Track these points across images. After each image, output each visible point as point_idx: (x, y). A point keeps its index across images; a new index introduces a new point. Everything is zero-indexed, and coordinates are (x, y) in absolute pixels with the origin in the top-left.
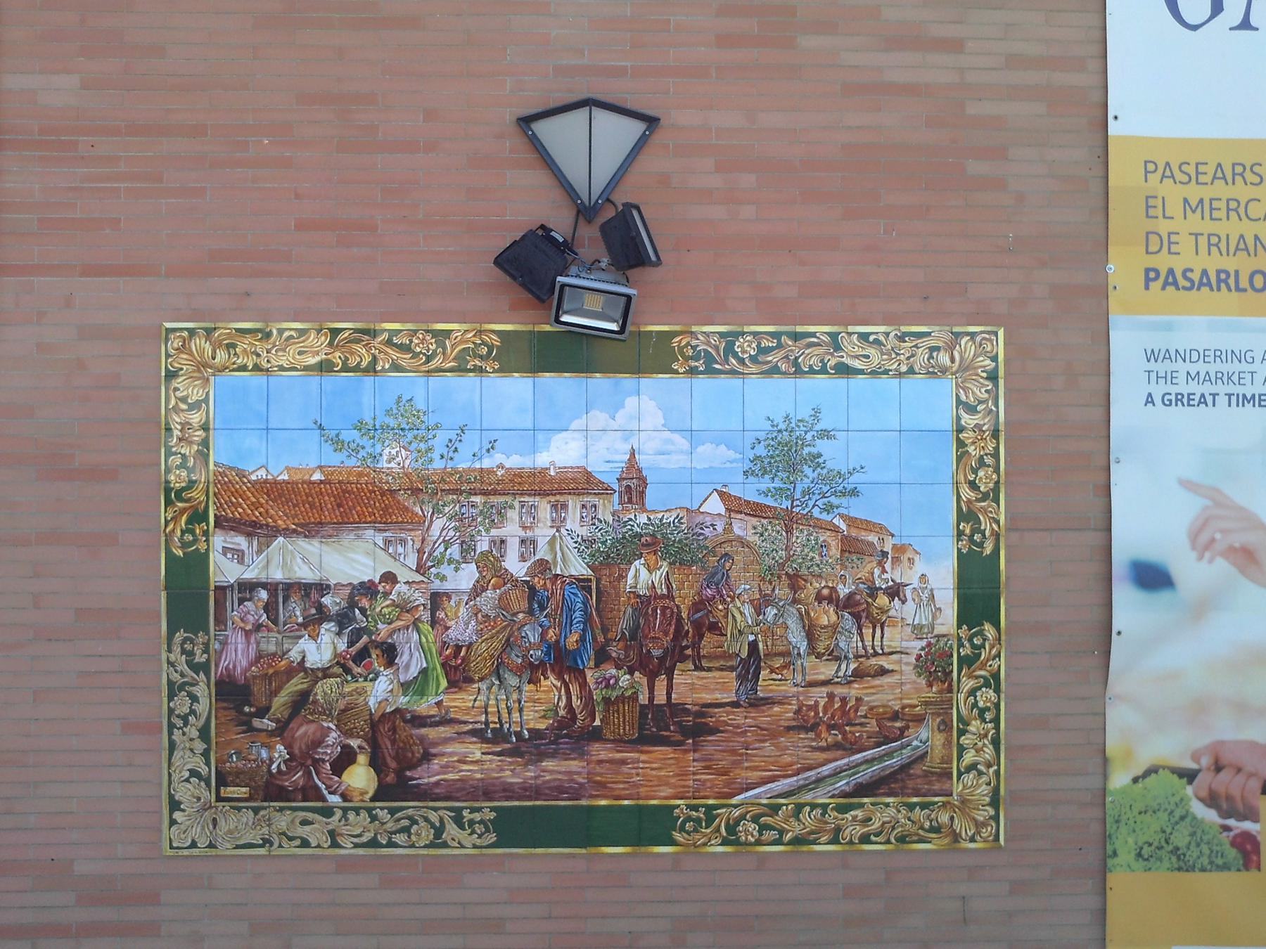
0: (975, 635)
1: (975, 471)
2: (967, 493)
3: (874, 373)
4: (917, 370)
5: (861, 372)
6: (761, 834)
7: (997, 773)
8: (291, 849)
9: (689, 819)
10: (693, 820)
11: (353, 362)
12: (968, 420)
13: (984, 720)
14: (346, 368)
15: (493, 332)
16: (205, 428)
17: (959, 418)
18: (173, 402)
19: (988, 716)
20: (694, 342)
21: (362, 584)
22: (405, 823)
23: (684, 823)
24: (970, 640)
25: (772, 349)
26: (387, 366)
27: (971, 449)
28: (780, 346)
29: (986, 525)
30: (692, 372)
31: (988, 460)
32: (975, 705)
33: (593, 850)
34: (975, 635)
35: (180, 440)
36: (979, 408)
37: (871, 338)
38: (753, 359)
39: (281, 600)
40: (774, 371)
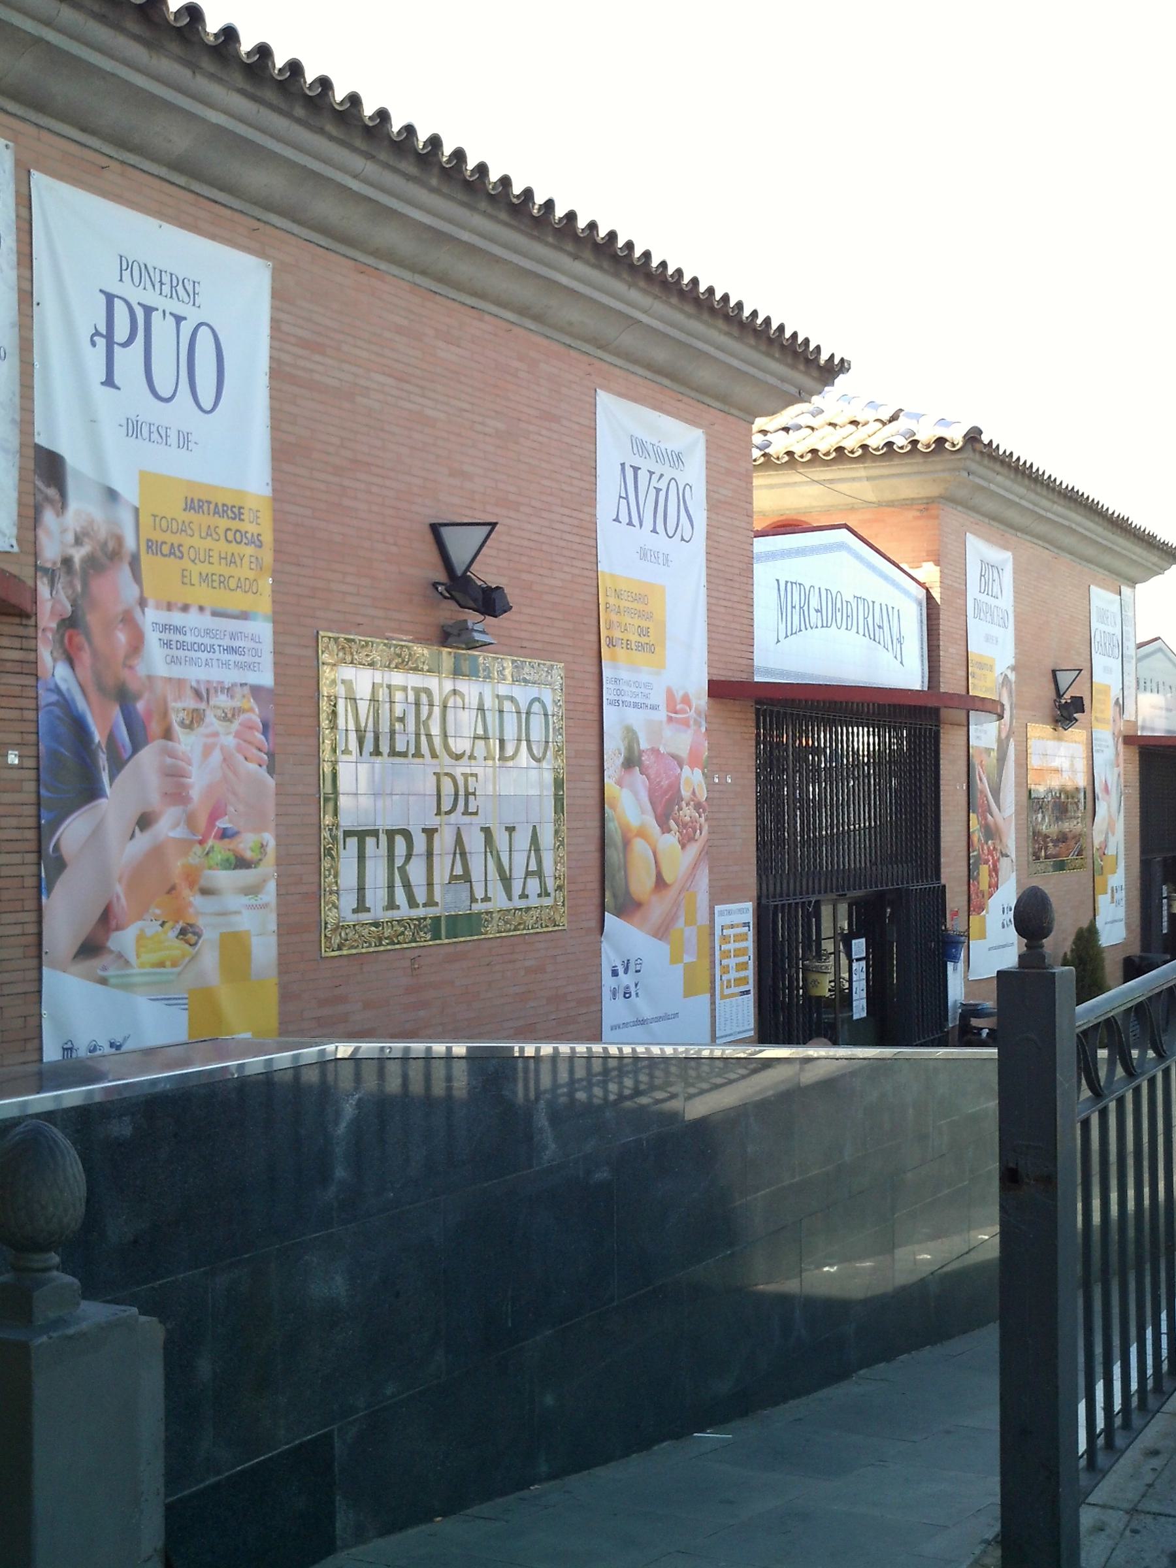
1: (332, 867)
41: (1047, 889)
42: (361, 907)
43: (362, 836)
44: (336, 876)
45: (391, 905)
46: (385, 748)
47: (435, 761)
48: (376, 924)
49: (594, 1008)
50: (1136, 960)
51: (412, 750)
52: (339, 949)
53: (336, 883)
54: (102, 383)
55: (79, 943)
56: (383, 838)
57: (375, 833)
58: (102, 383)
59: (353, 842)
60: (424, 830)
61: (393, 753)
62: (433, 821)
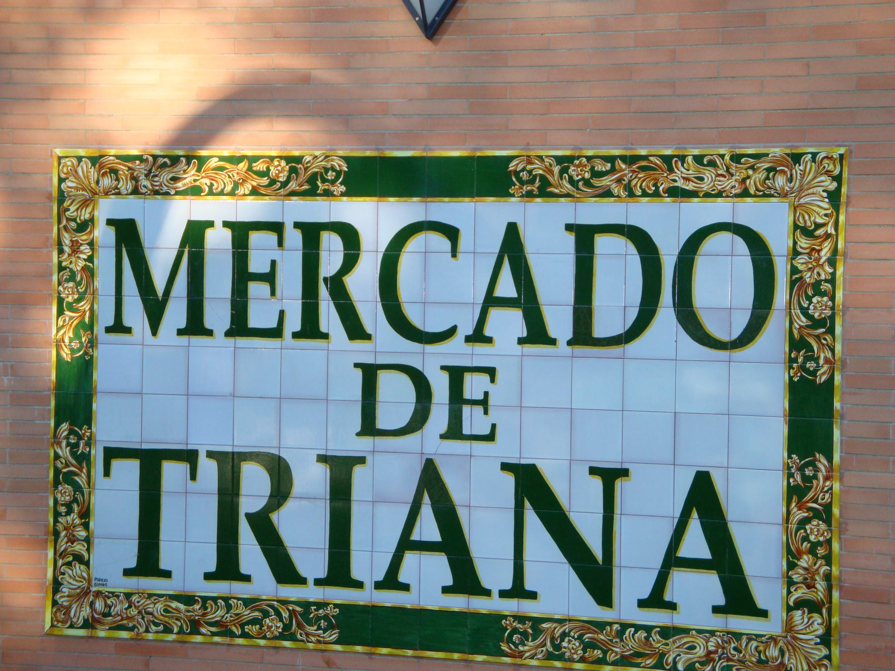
0: (807, 465)
1: (75, 500)
2: (81, 480)
3: (707, 195)
4: (752, 191)
5: (693, 194)
6: (585, 652)
7: (59, 222)
8: (711, 151)
9: (515, 631)
10: (520, 633)
11: (642, 634)
12: (80, 548)
13: (815, 555)
14: (211, 193)
15: (507, 655)
16: (790, 583)
17: (88, 550)
18: (64, 222)
19: (821, 551)
20: (67, 340)
21: (792, 448)
22: (595, 182)
23: (511, 635)
24: (801, 469)
25: (248, 623)
26: (608, 628)
27: (77, 521)
28: (613, 170)
29: (64, 452)
30: (530, 195)
31: (63, 509)
32: (806, 539)
33: (373, 650)
34: (807, 465)
35: (809, 587)
36: (71, 559)
37: (161, 628)
38: (587, 183)
39: (789, 144)
40: (607, 193)
41: (599, 608)
42: (148, 563)
43: (151, 462)
44: (85, 514)
45: (227, 567)
46: (217, 315)
47: (359, 345)
48: (188, 599)
49: (766, 311)
50: (48, 77)
51: (294, 322)
52: (61, 268)
53: (86, 526)
54: (358, 434)
55: (91, 514)
56: (208, 469)
57: (189, 457)
58: (358, 434)
59: (128, 472)
60: (128, 330)
61: (239, 327)
62: (347, 441)
